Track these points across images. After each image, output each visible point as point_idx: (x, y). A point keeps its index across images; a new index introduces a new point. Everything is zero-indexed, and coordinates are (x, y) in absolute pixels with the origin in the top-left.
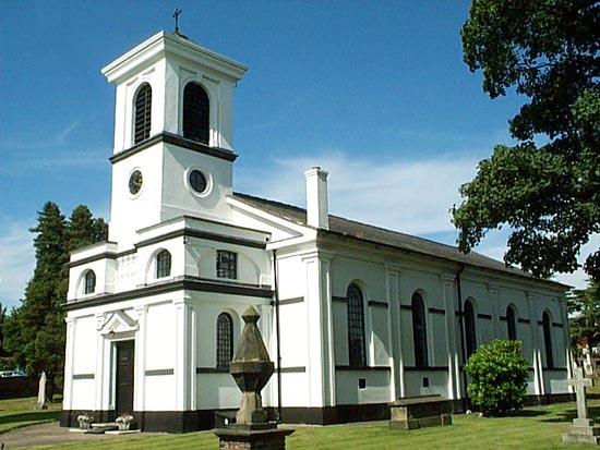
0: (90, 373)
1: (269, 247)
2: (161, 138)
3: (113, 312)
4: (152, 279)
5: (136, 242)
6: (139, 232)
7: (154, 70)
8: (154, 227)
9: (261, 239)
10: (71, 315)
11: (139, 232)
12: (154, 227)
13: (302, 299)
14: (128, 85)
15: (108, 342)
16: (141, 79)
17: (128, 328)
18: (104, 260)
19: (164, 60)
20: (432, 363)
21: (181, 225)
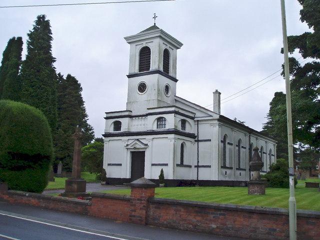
1: (196, 119)
4: (155, 128)
16: (144, 44)
17: (143, 146)
21: (173, 109)
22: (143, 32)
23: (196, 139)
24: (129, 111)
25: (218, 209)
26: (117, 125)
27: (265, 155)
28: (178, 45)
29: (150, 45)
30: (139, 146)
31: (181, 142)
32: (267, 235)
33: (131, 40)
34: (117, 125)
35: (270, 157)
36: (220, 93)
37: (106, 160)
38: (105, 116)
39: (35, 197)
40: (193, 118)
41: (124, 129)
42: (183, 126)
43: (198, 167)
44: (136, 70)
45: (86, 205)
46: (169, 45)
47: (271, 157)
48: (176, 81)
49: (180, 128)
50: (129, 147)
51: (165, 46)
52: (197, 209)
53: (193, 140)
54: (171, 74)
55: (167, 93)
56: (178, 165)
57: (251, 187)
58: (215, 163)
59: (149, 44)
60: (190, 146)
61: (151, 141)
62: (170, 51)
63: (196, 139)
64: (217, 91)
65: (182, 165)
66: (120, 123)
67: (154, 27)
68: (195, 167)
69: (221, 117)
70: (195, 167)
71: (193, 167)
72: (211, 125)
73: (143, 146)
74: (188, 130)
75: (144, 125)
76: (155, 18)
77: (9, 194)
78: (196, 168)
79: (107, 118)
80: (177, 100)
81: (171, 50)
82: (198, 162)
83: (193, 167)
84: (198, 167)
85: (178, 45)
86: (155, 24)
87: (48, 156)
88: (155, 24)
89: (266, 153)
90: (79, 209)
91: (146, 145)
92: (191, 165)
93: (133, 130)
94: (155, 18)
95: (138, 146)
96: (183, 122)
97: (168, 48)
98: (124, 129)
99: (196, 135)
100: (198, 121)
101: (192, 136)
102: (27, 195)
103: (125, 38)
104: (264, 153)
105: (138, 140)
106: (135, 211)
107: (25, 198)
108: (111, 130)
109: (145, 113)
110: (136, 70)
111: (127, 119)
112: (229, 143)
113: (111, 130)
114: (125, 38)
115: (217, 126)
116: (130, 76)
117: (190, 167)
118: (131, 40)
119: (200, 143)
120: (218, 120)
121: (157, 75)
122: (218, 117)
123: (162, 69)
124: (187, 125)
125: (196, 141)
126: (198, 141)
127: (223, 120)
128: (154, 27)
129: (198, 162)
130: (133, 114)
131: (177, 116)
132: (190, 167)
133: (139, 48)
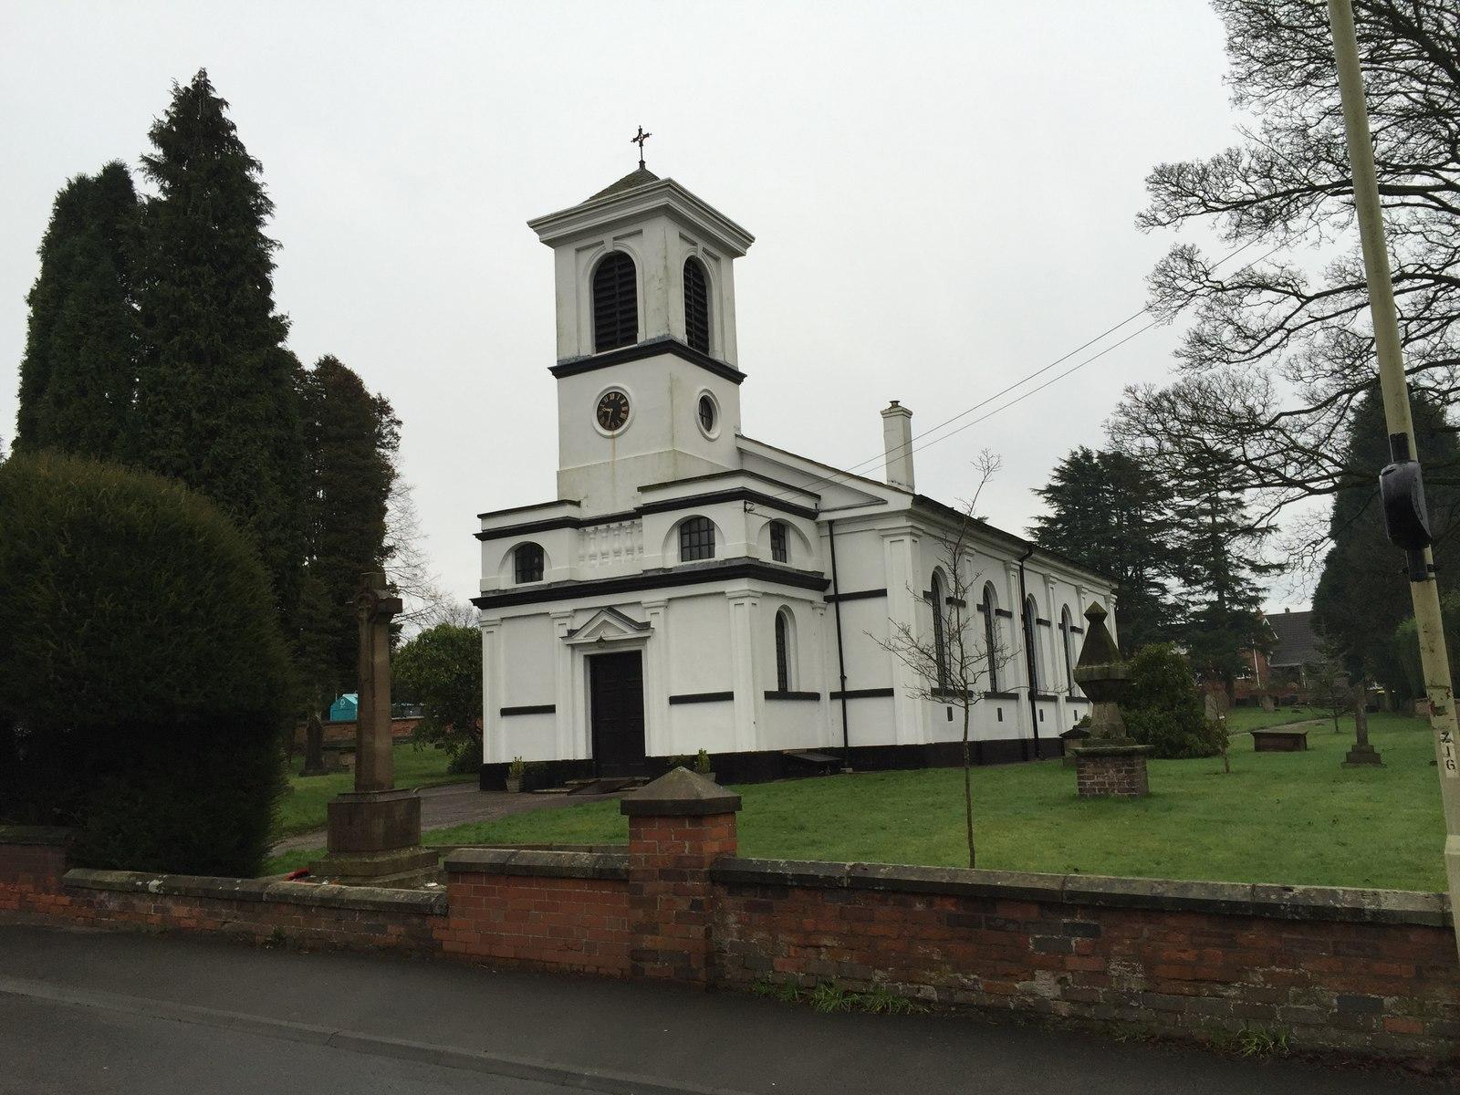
1: (824, 517)
3: (602, 609)
4: (671, 559)
6: (643, 489)
11: (643, 489)
14: (578, 250)
17: (631, 634)
22: (599, 195)
23: (831, 592)
25: (1050, 903)
26: (529, 561)
27: (1044, 629)
28: (733, 241)
29: (633, 248)
30: (616, 632)
31: (775, 605)
32: (1334, 1033)
34: (529, 561)
35: (989, 626)
36: (908, 414)
37: (495, 695)
38: (478, 527)
39: (185, 896)
40: (810, 514)
41: (554, 572)
42: (779, 545)
43: (843, 696)
44: (587, 349)
45: (419, 910)
46: (701, 244)
47: (1070, 634)
48: (736, 377)
49: (765, 555)
50: (580, 639)
51: (687, 246)
52: (949, 906)
53: (815, 596)
54: (718, 354)
55: (709, 426)
56: (769, 696)
57: (1090, 769)
58: (909, 679)
60: (810, 625)
62: (709, 264)
63: (831, 592)
64: (895, 404)
65: (782, 694)
66: (686, 552)
67: (642, 176)
68: (834, 696)
69: (921, 501)
70: (834, 696)
71: (825, 697)
72: (884, 534)
73: (631, 634)
74: (800, 559)
76: (641, 138)
77: (73, 889)
78: (840, 702)
79: (483, 537)
80: (746, 450)
81: (712, 262)
82: (843, 678)
83: (825, 697)
84: (843, 696)
85: (733, 241)
86: (642, 163)
88: (642, 163)
89: (1048, 624)
90: (394, 932)
91: (646, 626)
92: (817, 690)
94: (641, 138)
95: (610, 635)
96: (778, 532)
97: (700, 255)
98: (554, 572)
99: (828, 576)
100: (831, 523)
101: (813, 581)
102: (154, 883)
103: (536, 225)
104: (999, 612)
105: (611, 610)
106: (653, 930)
107: (144, 906)
108: (506, 580)
109: (628, 507)
110: (585, 347)
111: (567, 534)
112: (950, 601)
113: (506, 580)
114: (536, 225)
116: (561, 371)
117: (814, 697)
119: (846, 607)
121: (669, 361)
122: (905, 503)
123: (680, 335)
124: (793, 543)
125: (828, 599)
126: (837, 599)
127: (929, 513)
128: (642, 176)
129: (843, 678)
131: (758, 508)
132: (814, 697)
133: (590, 260)
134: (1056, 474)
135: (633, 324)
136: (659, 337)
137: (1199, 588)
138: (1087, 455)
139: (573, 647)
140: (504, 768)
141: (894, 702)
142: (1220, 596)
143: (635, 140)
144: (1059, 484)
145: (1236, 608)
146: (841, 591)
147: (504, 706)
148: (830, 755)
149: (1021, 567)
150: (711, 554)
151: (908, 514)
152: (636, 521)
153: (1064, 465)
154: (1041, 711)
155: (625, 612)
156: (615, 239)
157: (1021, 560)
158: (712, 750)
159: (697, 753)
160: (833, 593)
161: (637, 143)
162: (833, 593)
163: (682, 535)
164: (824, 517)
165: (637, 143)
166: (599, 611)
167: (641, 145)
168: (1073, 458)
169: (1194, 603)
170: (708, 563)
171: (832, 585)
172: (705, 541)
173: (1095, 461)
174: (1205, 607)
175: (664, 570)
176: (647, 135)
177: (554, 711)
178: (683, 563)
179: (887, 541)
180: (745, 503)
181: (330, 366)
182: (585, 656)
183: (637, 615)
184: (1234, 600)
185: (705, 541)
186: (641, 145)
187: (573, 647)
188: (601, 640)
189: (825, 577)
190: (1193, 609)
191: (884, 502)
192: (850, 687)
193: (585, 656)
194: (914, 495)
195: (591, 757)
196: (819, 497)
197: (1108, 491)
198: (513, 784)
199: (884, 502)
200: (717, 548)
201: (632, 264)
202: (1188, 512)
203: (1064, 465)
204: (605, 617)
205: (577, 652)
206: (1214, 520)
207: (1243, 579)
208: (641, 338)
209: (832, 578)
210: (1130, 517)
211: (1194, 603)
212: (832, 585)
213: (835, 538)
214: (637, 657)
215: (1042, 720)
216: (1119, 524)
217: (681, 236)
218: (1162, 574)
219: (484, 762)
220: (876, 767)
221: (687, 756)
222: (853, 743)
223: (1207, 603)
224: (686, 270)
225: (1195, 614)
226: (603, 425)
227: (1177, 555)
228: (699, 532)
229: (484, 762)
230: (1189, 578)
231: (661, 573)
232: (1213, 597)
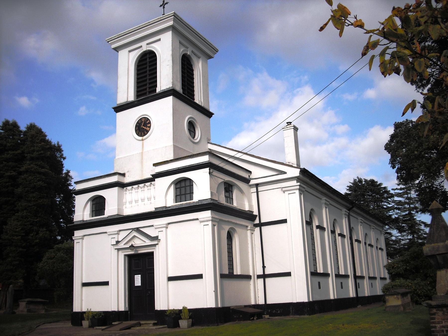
0: (371, 284)
1: (252, 182)
2: (172, 94)
3: (133, 229)
4: (170, 202)
5: (154, 173)
6: (155, 165)
7: (159, 40)
8: (171, 161)
9: (245, 175)
10: (78, 234)
11: (155, 165)
12: (171, 161)
13: (285, 221)
14: (130, 51)
15: (122, 255)
16: (144, 46)
17: (148, 242)
18: (116, 188)
19: (171, 31)
20: (238, 271)
21: (205, 159)
23: (257, 221)
24: (120, 174)
29: (157, 48)
31: (227, 228)
33: (417, 92)
40: (247, 181)
49: (222, 200)
50: (121, 245)
53: (249, 224)
59: (153, 45)
61: (164, 229)
63: (257, 221)
69: (304, 172)
70: (259, 277)
73: (148, 242)
75: (149, 199)
82: (264, 267)
84: (264, 276)
87: (63, 151)
91: (156, 238)
93: (128, 211)
95: (137, 243)
99: (256, 213)
100: (257, 185)
105: (138, 230)
115: (297, 192)
118: (417, 92)
119: (263, 228)
120: (297, 179)
122: (296, 173)
123: (179, 88)
125: (256, 225)
126: (261, 225)
129: (264, 267)
130: (127, 180)
131: (216, 173)
134: (348, 188)
135: (155, 84)
136: (167, 89)
137: (405, 234)
138: (360, 181)
139: (118, 250)
140: (81, 314)
141: (291, 277)
142: (413, 237)
143: (161, 6)
144: (350, 192)
145: (420, 241)
146: (263, 221)
147: (84, 281)
148: (257, 308)
149: (349, 213)
150: (191, 198)
151: (297, 179)
152: (153, 183)
153: (351, 184)
154: (358, 283)
155: (144, 230)
156: (148, 44)
157: (349, 210)
158: (189, 307)
159: (181, 308)
160: (258, 222)
161: (162, 7)
162: (258, 222)
163: (176, 189)
164: (252, 182)
165: (162, 7)
166: (131, 230)
167: (164, 8)
168: (355, 182)
169: (403, 240)
170: (190, 203)
171: (258, 218)
172: (188, 192)
173: (363, 183)
174: (408, 241)
175: (166, 207)
176: (167, 3)
177: (108, 285)
178: (177, 204)
179: (287, 193)
180: (210, 170)
181: (32, 127)
182: (125, 255)
183: (151, 232)
184: (419, 238)
185: (188, 192)
186: (164, 8)
187: (118, 250)
188: (132, 246)
189: (254, 213)
190: (403, 242)
191: (285, 173)
192: (267, 272)
193: (125, 255)
194: (301, 168)
195: (127, 309)
196: (250, 172)
197: (369, 195)
198: (85, 323)
199: (285, 173)
200: (194, 195)
201: (155, 56)
202: (399, 203)
203: (351, 184)
204: (135, 234)
205: (120, 252)
206: (410, 206)
207: (421, 230)
208: (158, 90)
209: (257, 214)
210: (378, 206)
211: (403, 240)
212: (258, 218)
213: (260, 193)
214: (151, 254)
215: (359, 288)
216: (374, 208)
217: (180, 43)
218: (391, 228)
219: (74, 311)
220: (220, 158)
221: (176, 310)
222: (269, 302)
223: (408, 239)
224: (182, 59)
225: (404, 244)
226: (138, 134)
227: (396, 220)
228: (185, 187)
229: (74, 311)
230: (401, 230)
231: (164, 209)
232: (409, 237)
